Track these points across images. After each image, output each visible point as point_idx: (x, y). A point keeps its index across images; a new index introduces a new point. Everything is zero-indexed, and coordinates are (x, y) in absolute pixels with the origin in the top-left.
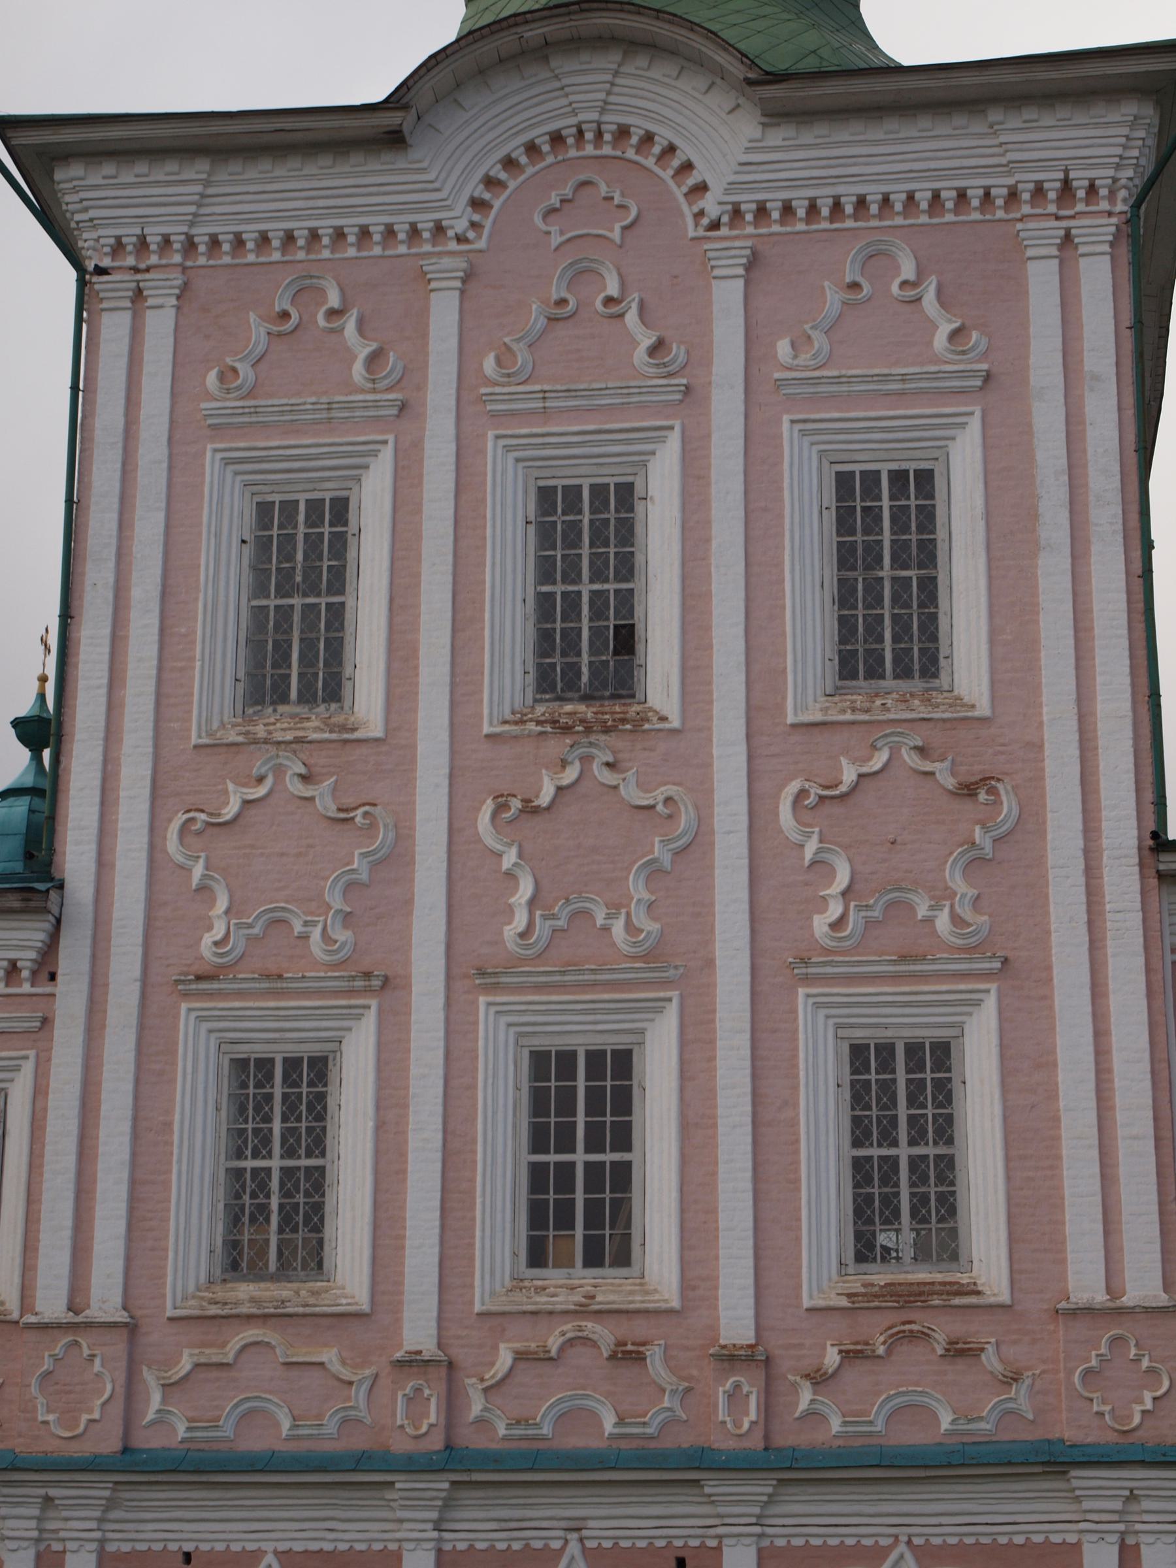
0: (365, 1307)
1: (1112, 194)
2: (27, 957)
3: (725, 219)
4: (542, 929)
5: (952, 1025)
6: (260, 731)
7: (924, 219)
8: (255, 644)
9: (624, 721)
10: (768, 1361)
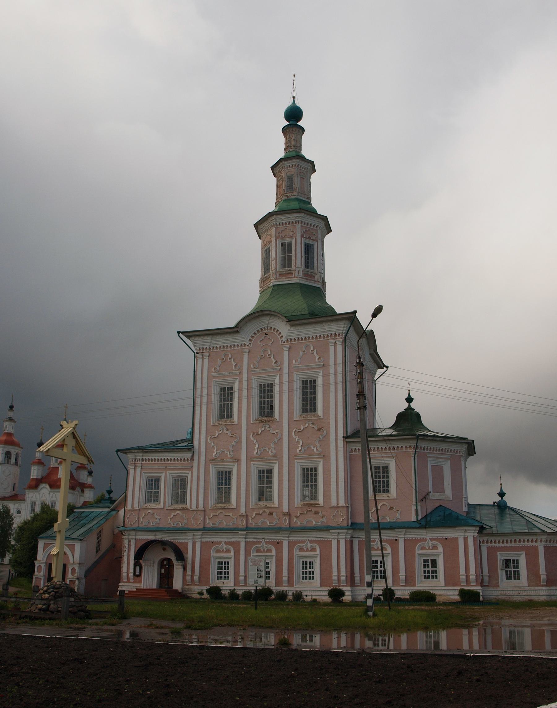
0: (236, 507)
1: (342, 335)
2: (189, 457)
3: (286, 341)
4: (259, 452)
5: (317, 465)
6: (221, 423)
7: (315, 340)
8: (220, 409)
9: (271, 420)
10: (290, 515)
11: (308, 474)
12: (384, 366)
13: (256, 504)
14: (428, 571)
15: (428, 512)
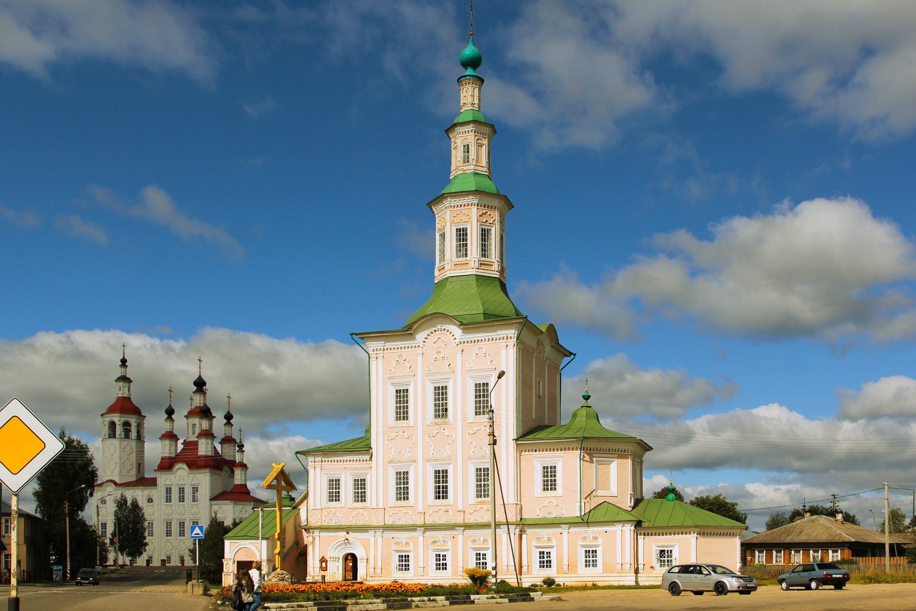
2: (368, 459)
11: (481, 474)
12: (571, 354)
14: (405, 561)
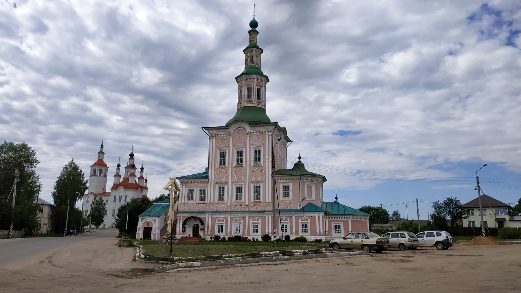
4: (237, 180)
12: (291, 141)
13: (235, 201)
15: (305, 205)
